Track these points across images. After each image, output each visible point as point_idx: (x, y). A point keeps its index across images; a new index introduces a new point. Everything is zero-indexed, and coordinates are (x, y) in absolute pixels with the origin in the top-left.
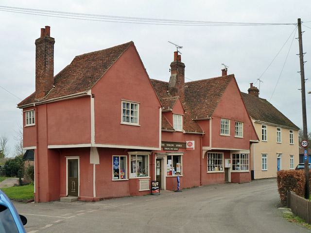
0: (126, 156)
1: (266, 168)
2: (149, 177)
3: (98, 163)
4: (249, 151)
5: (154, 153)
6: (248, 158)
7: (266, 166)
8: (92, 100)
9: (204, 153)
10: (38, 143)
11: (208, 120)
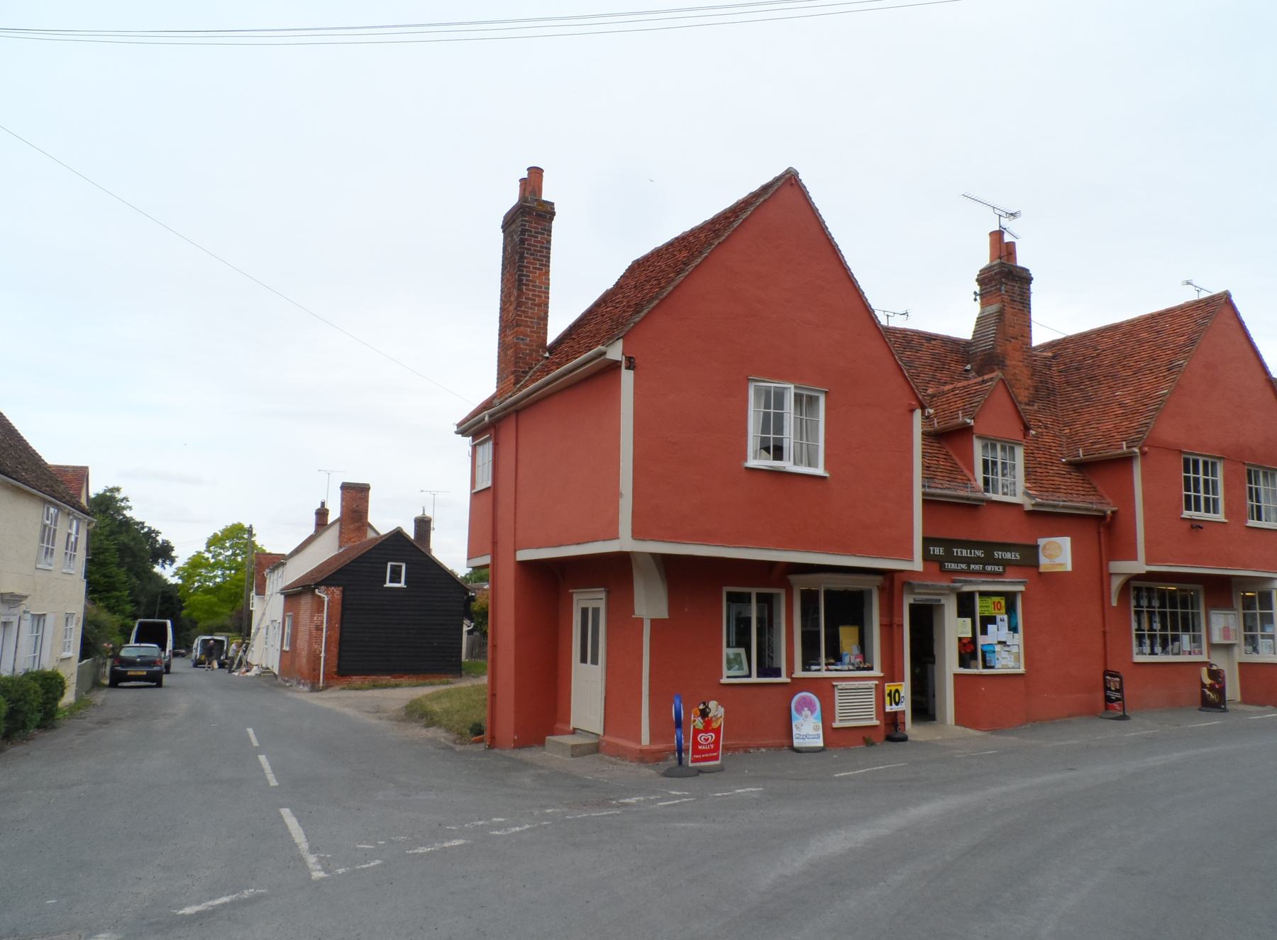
3: (664, 614)
5: (897, 583)
8: (627, 377)
9: (1116, 583)
10: (495, 543)
11: (1127, 460)
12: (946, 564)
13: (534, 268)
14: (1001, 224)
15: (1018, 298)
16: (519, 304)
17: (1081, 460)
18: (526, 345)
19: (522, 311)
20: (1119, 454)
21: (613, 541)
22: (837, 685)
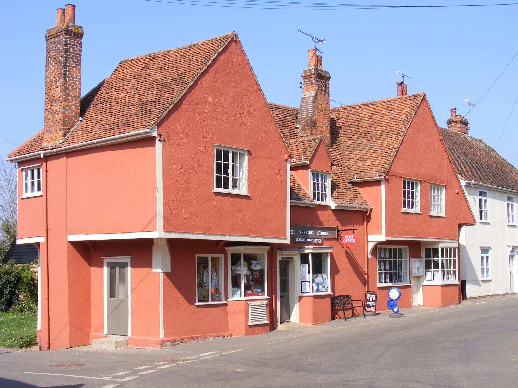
0: (222, 256)
1: (487, 276)
2: (266, 296)
4: (256, 261)
6: (454, 256)
7: (487, 272)
12: (296, 239)
13: (73, 67)
14: (316, 47)
15: (323, 88)
16: (65, 88)
17: (356, 181)
18: (69, 113)
19: (66, 93)
20: (375, 179)
21: (460, 260)
22: (250, 304)
